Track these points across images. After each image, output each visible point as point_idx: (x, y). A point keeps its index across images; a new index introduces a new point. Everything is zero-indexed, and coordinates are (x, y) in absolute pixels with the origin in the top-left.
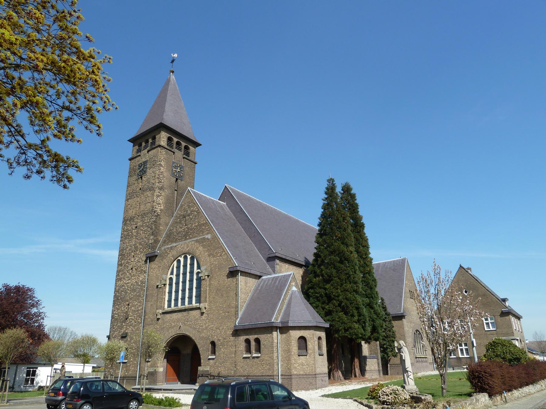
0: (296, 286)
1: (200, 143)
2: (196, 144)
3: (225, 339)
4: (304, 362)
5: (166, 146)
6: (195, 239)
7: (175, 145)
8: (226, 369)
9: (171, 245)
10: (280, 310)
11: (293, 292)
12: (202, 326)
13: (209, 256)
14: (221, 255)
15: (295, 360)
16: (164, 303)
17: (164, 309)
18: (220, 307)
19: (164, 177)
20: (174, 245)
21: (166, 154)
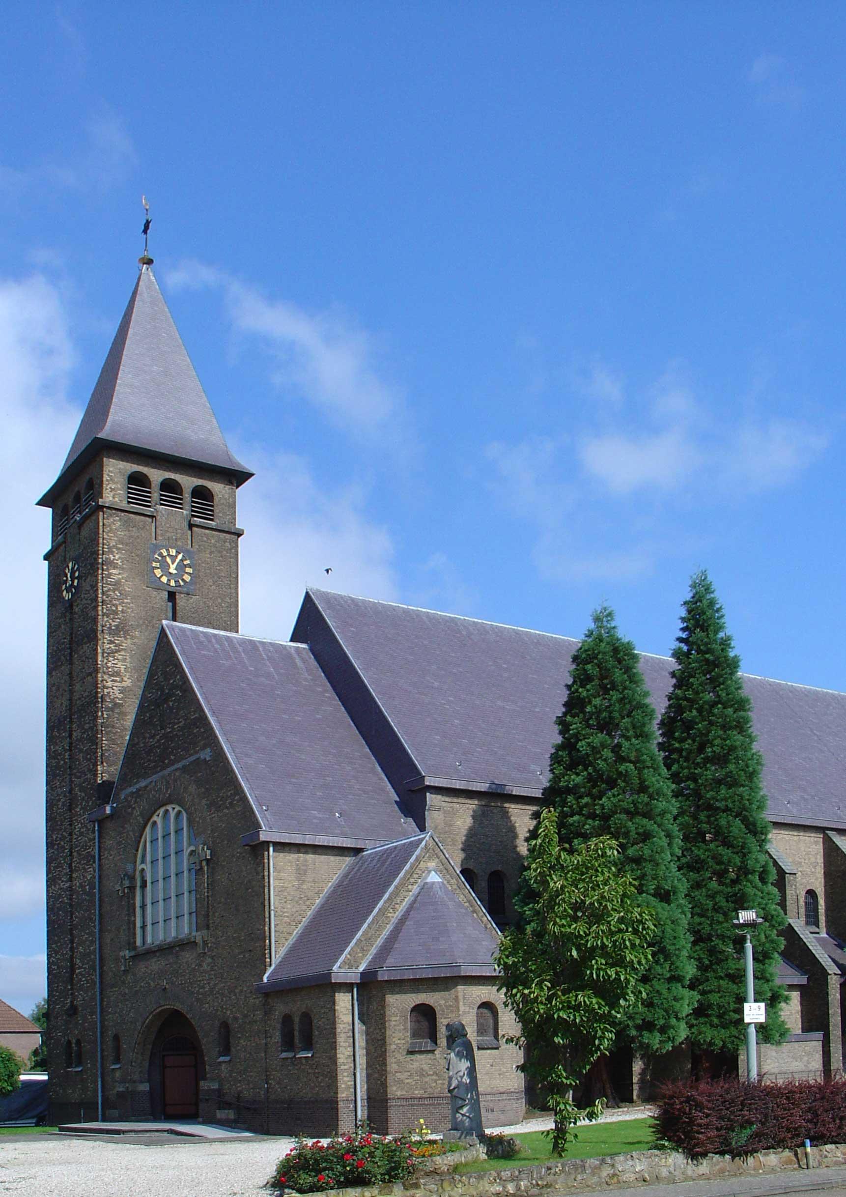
0: (444, 869)
1: (252, 470)
2: (237, 477)
3: (246, 1016)
4: (426, 1067)
5: (124, 505)
6: (180, 765)
7: (156, 495)
8: (251, 1086)
9: (137, 786)
10: (369, 939)
11: (426, 889)
12: (203, 987)
13: (210, 806)
14: (231, 803)
15: (399, 1063)
16: (135, 934)
17: (135, 948)
18: (234, 938)
19: (124, 595)
20: (143, 784)
21: (126, 524)
